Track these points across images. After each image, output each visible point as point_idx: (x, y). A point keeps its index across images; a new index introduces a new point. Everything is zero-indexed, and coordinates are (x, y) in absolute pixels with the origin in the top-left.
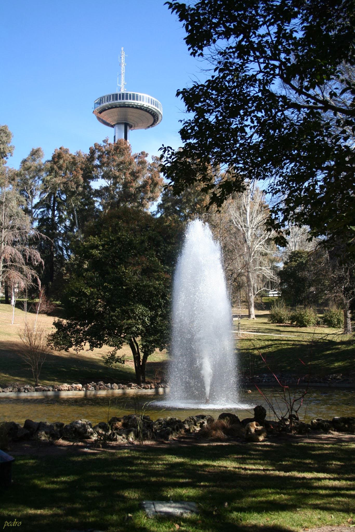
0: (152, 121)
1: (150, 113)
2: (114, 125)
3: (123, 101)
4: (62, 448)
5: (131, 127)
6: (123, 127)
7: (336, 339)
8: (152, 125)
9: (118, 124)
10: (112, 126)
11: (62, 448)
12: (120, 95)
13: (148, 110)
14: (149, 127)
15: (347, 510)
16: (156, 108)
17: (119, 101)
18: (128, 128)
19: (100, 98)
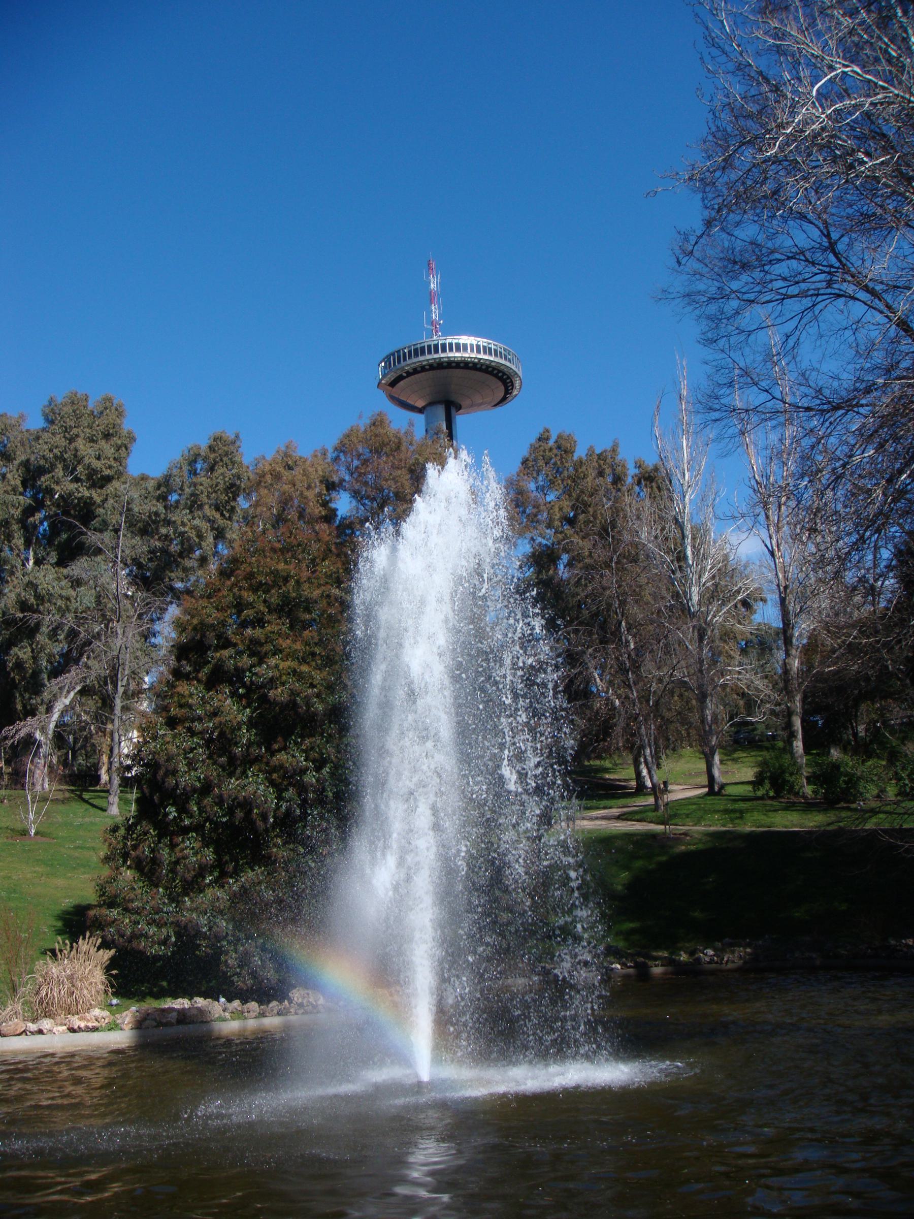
0: (501, 393)
1: (480, 370)
2: (424, 408)
3: (436, 356)
4: (40, 1181)
5: (459, 408)
6: (440, 411)
7: (251, 789)
8: (504, 400)
9: (431, 404)
10: (420, 411)
11: (40, 1181)
12: (429, 347)
13: (479, 366)
14: (495, 405)
15: (4, 1063)
16: (508, 364)
17: (428, 357)
18: (453, 410)
19: (388, 357)
